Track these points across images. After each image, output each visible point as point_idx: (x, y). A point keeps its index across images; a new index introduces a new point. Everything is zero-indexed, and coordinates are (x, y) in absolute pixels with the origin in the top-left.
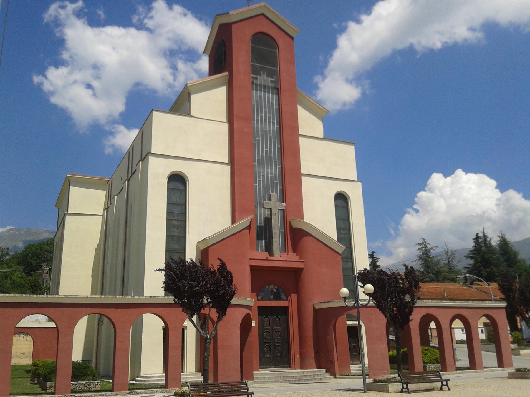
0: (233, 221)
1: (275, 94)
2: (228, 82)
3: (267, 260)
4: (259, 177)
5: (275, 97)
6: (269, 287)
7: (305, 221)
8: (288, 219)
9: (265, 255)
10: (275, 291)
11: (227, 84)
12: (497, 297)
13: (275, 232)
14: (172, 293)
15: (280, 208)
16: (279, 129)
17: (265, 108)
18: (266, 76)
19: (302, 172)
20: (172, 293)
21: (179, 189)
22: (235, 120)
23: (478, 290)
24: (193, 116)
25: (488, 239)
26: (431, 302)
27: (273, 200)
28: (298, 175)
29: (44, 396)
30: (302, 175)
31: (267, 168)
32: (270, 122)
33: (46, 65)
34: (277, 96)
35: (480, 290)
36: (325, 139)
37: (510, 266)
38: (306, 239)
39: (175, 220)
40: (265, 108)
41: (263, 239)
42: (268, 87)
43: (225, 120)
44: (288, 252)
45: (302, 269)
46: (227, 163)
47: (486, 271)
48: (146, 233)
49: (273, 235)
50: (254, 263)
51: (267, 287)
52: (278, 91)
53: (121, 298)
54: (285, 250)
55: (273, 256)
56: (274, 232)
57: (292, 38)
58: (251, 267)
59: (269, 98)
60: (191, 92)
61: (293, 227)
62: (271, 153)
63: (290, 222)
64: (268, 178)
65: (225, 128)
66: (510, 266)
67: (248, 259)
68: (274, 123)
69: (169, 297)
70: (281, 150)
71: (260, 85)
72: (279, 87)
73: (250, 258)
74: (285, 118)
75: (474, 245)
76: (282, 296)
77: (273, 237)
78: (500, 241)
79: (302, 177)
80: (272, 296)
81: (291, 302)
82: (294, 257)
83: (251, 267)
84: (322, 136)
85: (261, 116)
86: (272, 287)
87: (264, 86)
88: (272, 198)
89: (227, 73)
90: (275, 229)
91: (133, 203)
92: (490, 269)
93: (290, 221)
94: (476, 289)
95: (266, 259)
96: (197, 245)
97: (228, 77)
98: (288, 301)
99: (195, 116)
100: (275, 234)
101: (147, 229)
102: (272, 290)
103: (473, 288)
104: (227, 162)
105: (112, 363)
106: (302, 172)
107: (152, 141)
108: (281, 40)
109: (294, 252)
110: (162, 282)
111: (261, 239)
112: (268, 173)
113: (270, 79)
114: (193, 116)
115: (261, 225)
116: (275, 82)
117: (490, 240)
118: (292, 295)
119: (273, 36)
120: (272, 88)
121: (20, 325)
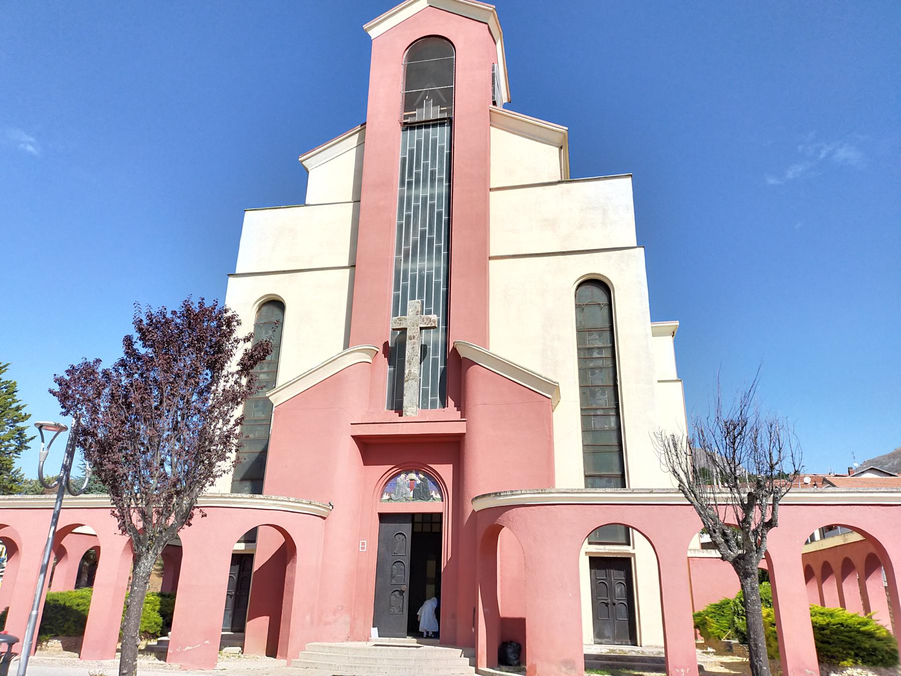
14: (134, 664)
17: (426, 158)
20: (134, 664)
29: (304, 207)
31: (422, 260)
33: (839, 670)
40: (426, 158)
56: (407, 372)
62: (431, 232)
64: (421, 277)
68: (441, 180)
77: (406, 379)
85: (418, 175)
91: (720, 399)
100: (410, 372)
105: (40, 589)
110: (11, 380)
112: (421, 270)
116: (242, 340)
121: (73, 531)
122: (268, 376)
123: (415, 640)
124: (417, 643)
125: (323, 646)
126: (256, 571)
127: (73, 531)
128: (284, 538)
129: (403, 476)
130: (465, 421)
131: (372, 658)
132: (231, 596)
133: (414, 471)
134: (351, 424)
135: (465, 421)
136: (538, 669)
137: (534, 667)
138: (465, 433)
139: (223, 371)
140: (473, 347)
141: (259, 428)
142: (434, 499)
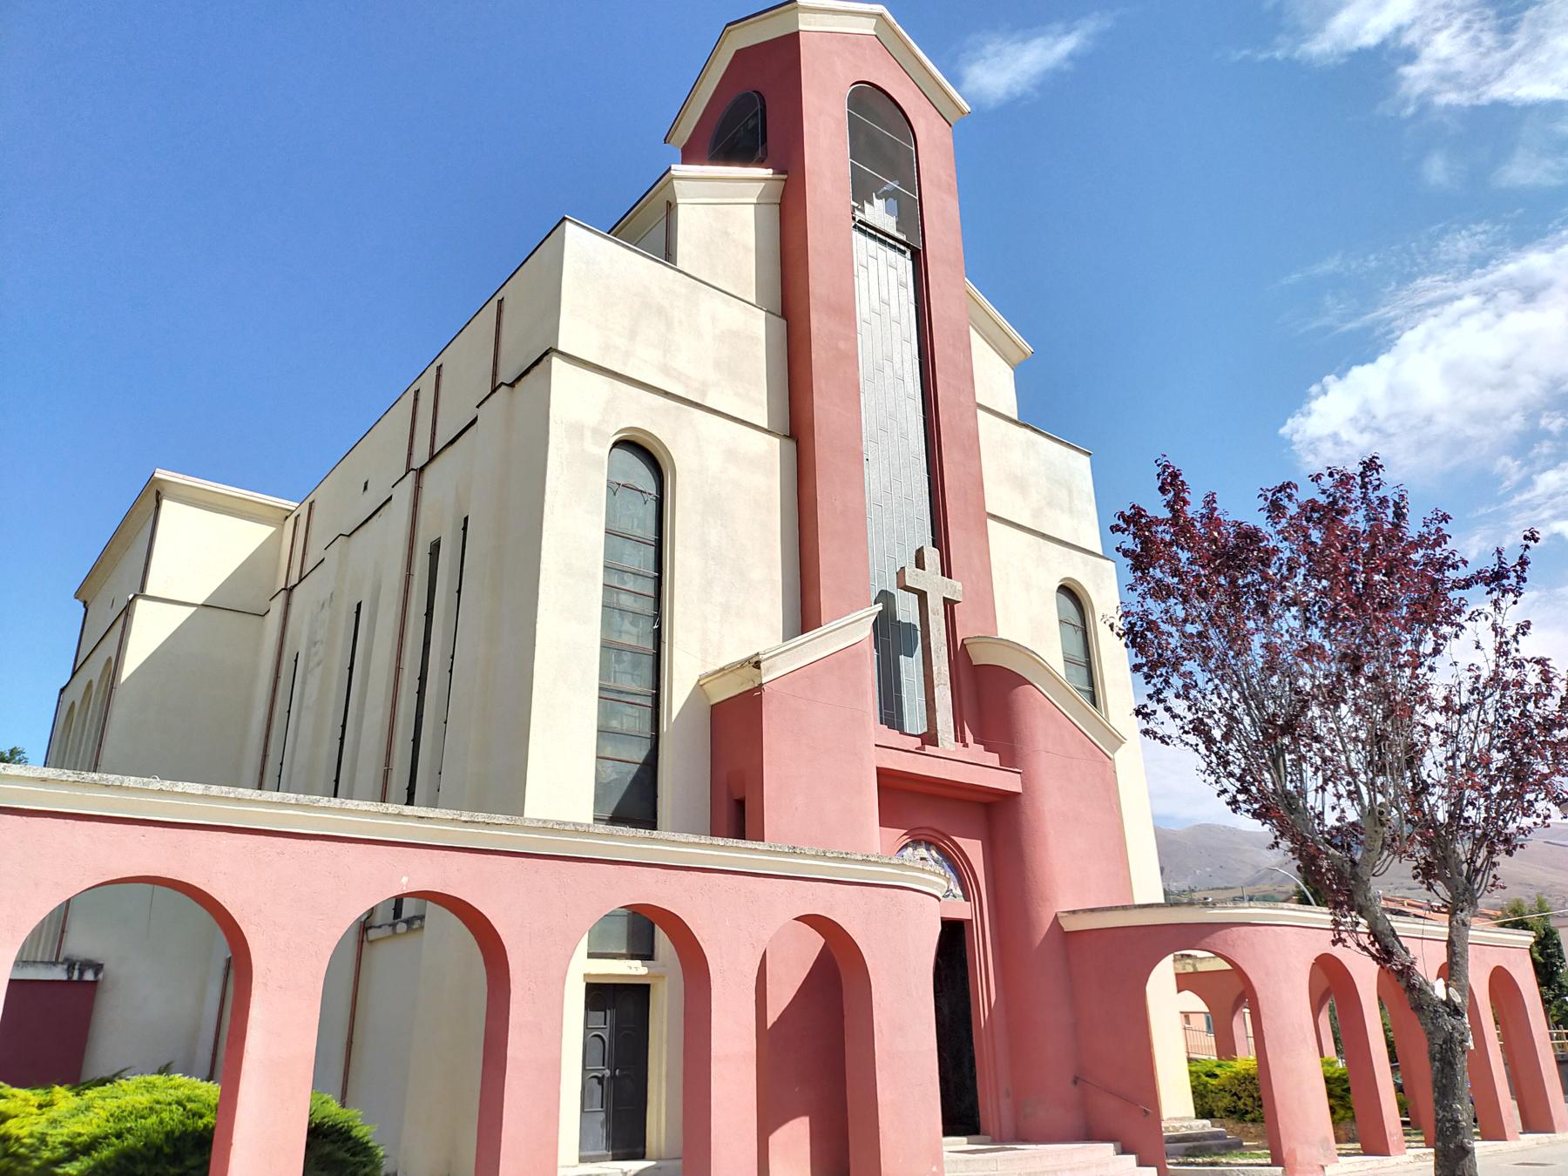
122: (635, 601)
123: (964, 1139)
124: (968, 1143)
125: (953, 1161)
126: (775, 1024)
127: (1229, 967)
128: (1203, 970)
129: (910, 850)
130: (1019, 773)
131: (1050, 1171)
132: (600, 1080)
133: (923, 843)
134: (876, 745)
135: (1019, 773)
136: (1299, 1156)
137: (1292, 1152)
138: (1019, 793)
139: (1277, 679)
140: (1034, 656)
141: (629, 710)
142: (954, 896)
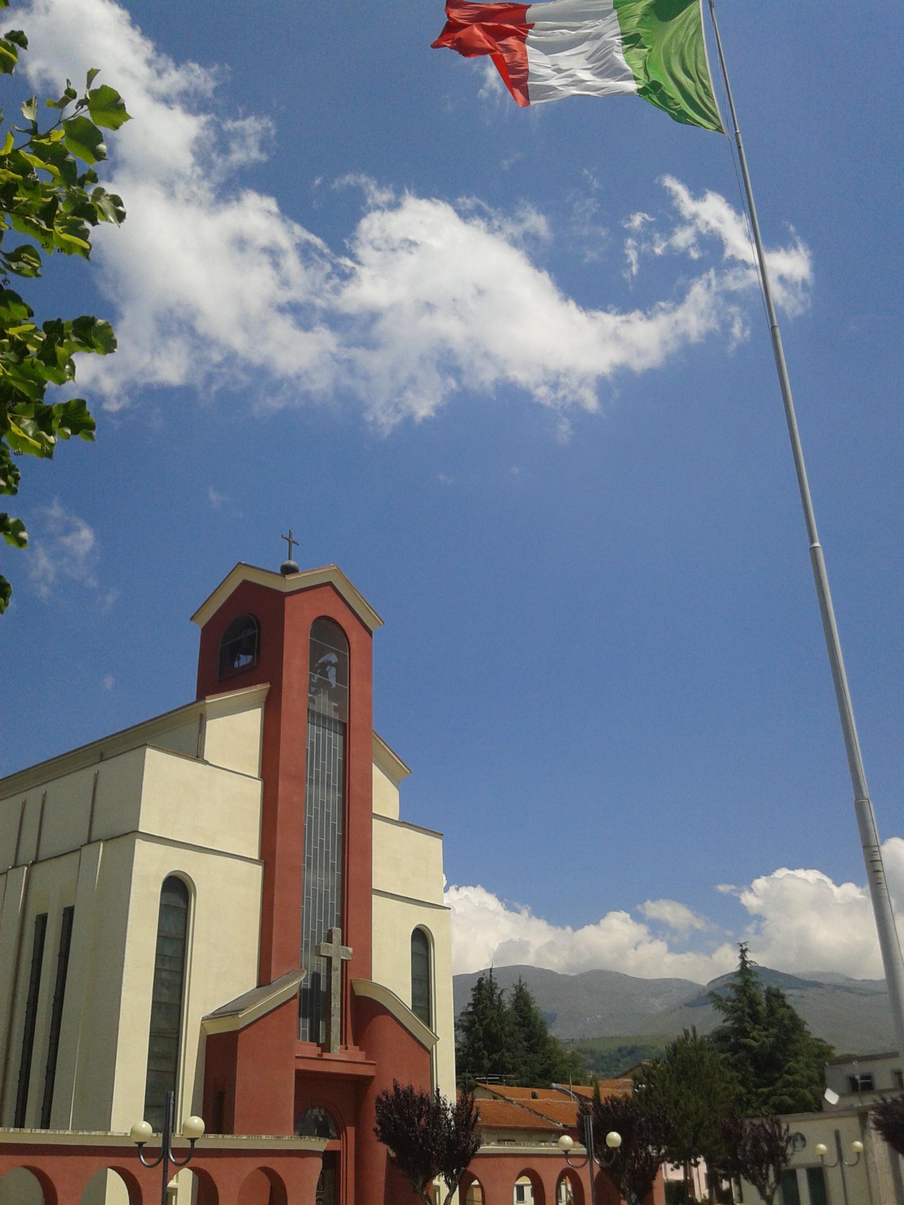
0: (264, 979)
1: (339, 734)
2: (264, 700)
3: (319, 1058)
4: (308, 894)
5: (339, 738)
6: (312, 1112)
7: (374, 981)
8: (349, 978)
9: (312, 1050)
10: (321, 1119)
11: (263, 704)
12: (559, 1123)
13: (335, 1004)
15: (345, 956)
16: (341, 800)
18: (327, 698)
19: (373, 887)
21: (175, 907)
22: (280, 777)
23: (523, 1107)
24: (207, 763)
25: (498, 992)
26: (545, 1146)
27: (334, 942)
28: (368, 891)
30: (374, 892)
32: (328, 786)
34: (342, 737)
35: (528, 1108)
36: (401, 823)
37: (531, 1049)
38: (381, 1019)
39: (166, 970)
41: (308, 1015)
42: (330, 719)
43: (255, 771)
44: (213, 1018)
45: (372, 1077)
46: (257, 860)
47: (490, 1060)
48: (122, 996)
49: (332, 1009)
50: (304, 1066)
51: (309, 1112)
52: (345, 729)
53: (154, 1137)
54: (343, 1041)
55: (330, 1052)
56: (333, 1004)
57: (370, 632)
58: (298, 1072)
59: (330, 739)
60: (208, 715)
61: (357, 994)
63: (351, 984)
65: (255, 789)
66: (531, 1049)
67: (294, 1058)
68: (334, 787)
69: (225, 1137)
70: (344, 840)
71: (319, 715)
72: (348, 723)
73: (297, 1055)
74: (354, 781)
75: (473, 1002)
76: (331, 1131)
78: (515, 997)
79: (373, 895)
80: (316, 1131)
81: (345, 1142)
82: (360, 1056)
83: (298, 1072)
84: (396, 817)
86: (316, 1111)
87: (325, 718)
88: (334, 937)
89: (266, 686)
90: (335, 998)
92: (499, 1054)
93: (352, 982)
94: (520, 1105)
95: (316, 1057)
96: (202, 1024)
97: (268, 689)
98: (340, 1139)
99: (210, 762)
101: (123, 988)
102: (316, 1118)
103: (514, 1102)
104: (256, 857)
106: (373, 887)
107: (142, 807)
108: (355, 635)
109: (356, 1044)
111: (305, 1017)
113: (334, 704)
114: (207, 763)
115: (306, 987)
117: (501, 994)
118: (348, 1128)
119: (343, 625)
120: (335, 721)
